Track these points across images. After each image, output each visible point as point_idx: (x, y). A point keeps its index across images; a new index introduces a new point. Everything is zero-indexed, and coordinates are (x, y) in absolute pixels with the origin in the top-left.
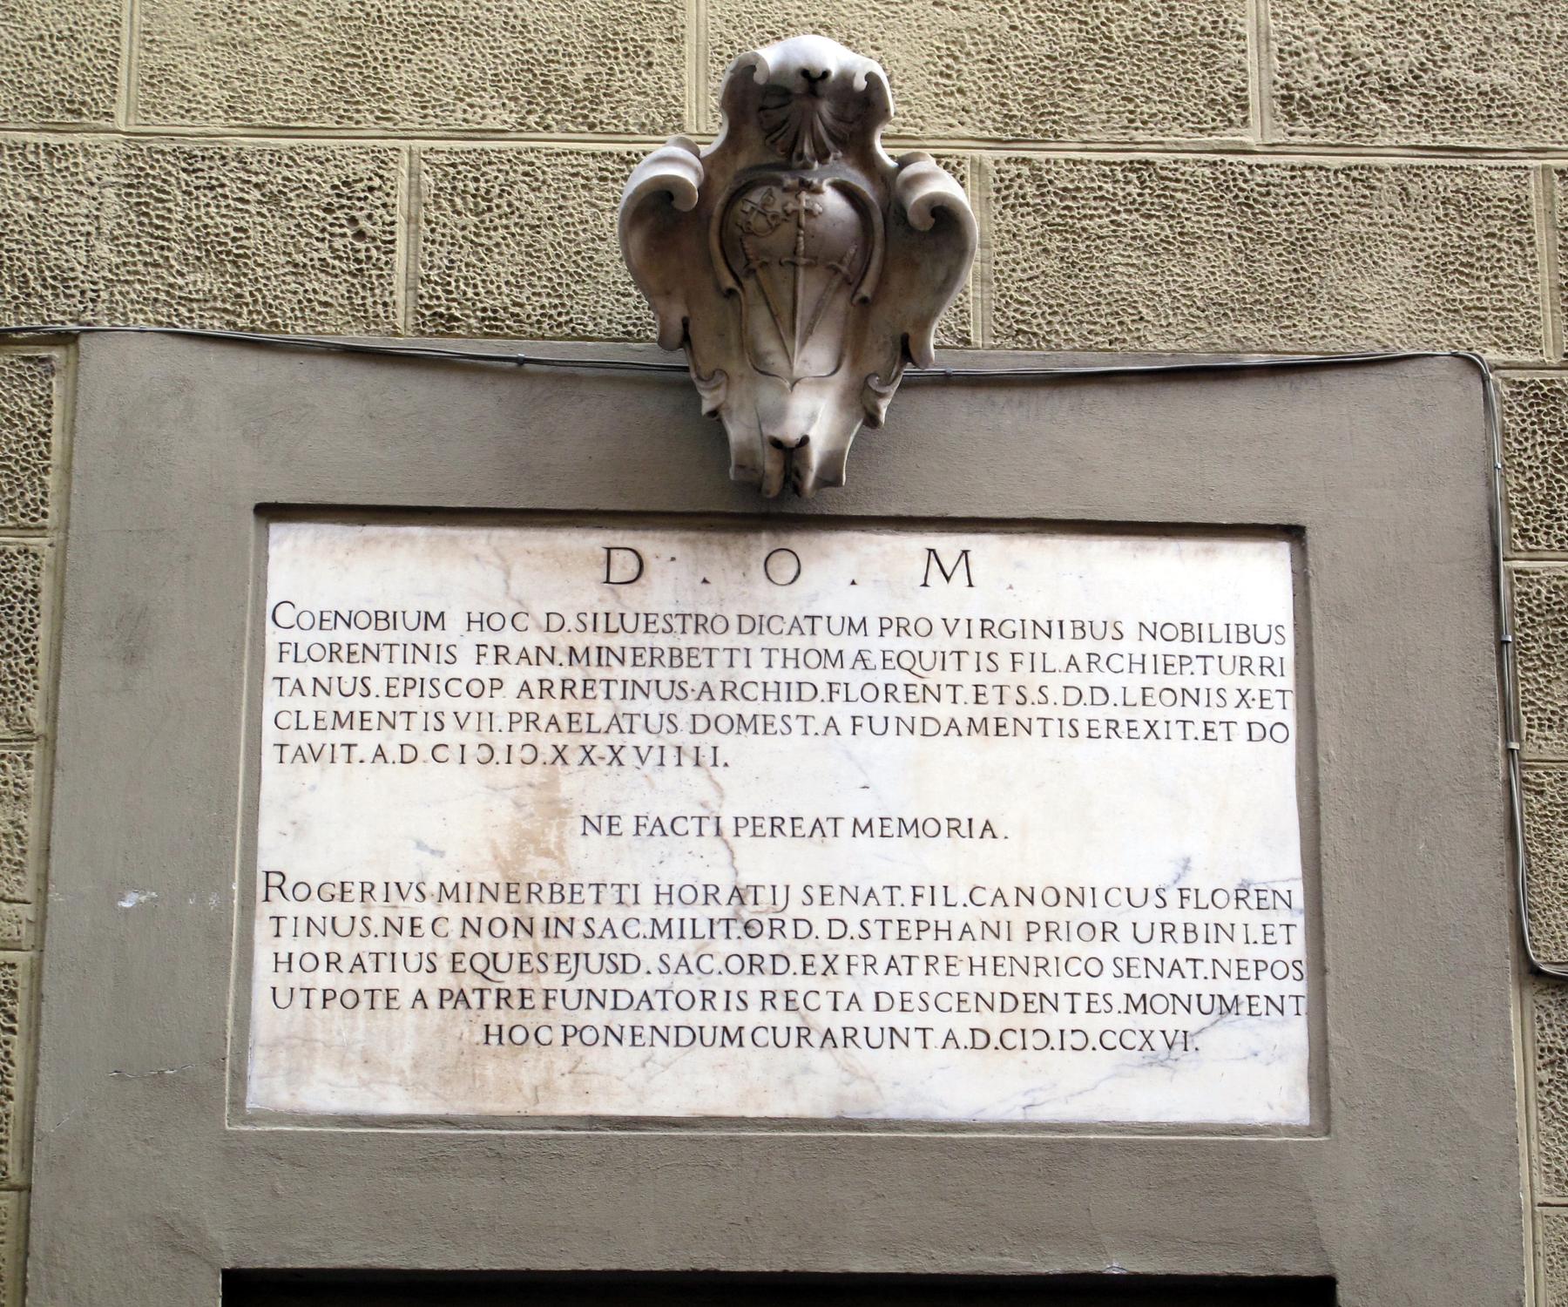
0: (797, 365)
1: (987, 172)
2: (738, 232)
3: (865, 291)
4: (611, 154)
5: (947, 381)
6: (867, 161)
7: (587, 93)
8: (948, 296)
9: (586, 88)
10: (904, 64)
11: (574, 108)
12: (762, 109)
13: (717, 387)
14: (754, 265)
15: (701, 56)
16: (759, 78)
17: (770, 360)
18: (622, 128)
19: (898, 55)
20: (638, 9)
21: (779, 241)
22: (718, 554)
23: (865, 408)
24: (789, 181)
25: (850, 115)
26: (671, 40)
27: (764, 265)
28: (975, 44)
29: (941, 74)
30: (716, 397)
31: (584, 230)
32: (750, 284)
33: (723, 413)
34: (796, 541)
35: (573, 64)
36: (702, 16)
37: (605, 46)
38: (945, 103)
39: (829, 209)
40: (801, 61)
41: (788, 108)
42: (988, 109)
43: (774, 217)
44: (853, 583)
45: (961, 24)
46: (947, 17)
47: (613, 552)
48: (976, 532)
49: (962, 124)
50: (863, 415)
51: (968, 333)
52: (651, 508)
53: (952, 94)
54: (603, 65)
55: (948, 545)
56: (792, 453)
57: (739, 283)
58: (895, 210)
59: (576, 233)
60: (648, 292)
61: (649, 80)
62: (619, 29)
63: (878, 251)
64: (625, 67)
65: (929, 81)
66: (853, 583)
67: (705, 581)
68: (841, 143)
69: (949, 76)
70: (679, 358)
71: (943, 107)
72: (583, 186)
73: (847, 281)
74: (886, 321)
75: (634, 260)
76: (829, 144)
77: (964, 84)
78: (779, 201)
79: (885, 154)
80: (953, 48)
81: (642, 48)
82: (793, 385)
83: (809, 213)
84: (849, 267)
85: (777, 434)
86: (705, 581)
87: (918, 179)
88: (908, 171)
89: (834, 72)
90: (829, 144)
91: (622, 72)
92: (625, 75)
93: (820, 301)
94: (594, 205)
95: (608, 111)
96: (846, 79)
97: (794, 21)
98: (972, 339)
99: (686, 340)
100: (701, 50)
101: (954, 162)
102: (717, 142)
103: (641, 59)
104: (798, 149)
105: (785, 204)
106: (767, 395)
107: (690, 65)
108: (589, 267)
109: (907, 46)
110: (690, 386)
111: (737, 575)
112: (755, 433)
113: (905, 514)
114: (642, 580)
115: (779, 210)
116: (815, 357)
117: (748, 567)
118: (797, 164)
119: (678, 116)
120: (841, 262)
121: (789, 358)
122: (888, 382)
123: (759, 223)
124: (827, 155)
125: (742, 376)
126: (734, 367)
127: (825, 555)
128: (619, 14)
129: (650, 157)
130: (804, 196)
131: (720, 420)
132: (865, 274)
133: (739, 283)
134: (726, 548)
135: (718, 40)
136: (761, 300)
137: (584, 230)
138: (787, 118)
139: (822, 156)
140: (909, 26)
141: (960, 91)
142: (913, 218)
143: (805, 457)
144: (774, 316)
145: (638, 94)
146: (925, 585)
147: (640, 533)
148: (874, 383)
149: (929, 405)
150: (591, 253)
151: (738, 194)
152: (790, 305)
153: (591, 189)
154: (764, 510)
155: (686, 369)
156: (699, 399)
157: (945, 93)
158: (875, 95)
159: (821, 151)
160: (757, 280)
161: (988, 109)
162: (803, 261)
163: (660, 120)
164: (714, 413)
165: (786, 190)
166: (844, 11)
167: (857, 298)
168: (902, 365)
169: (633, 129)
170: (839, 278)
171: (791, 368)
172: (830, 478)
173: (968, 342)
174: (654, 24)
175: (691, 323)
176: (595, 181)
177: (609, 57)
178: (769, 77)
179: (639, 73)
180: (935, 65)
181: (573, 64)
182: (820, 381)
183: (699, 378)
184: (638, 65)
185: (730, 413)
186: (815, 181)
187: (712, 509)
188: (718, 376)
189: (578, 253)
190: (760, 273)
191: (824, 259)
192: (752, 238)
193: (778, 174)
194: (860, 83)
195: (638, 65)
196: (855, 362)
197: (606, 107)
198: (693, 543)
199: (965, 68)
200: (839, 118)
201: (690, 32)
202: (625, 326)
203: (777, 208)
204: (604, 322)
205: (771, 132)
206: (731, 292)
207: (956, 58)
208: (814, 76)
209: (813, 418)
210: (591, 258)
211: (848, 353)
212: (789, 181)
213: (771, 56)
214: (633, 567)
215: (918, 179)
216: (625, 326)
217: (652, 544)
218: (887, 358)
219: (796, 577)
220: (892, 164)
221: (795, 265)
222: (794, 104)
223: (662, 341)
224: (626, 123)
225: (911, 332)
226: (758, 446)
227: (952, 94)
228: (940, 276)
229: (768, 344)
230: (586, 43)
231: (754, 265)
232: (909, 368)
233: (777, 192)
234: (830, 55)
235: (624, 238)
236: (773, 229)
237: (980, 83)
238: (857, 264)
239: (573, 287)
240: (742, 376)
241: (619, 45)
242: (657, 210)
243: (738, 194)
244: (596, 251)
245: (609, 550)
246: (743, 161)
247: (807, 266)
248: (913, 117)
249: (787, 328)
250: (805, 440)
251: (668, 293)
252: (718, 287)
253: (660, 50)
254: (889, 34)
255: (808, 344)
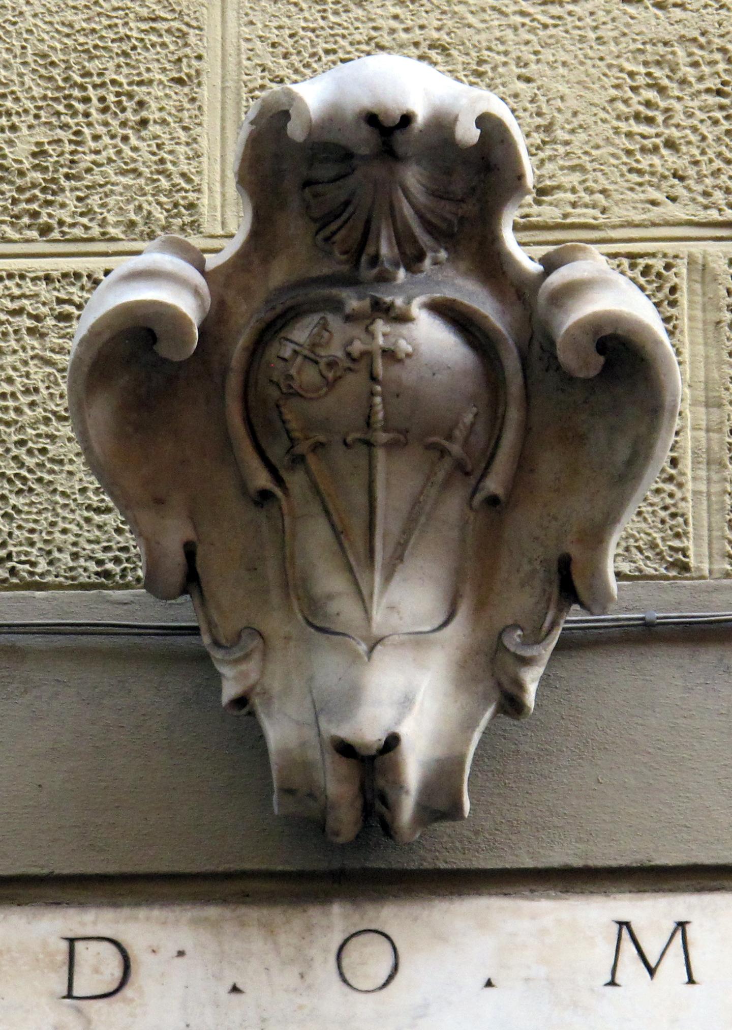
0: (378, 615)
1: (715, 279)
2: (274, 393)
3: (494, 484)
4: (78, 276)
5: (647, 634)
6: (491, 265)
7: (38, 176)
8: (634, 489)
9: (35, 167)
10: (573, 103)
11: (15, 201)
12: (308, 183)
13: (246, 657)
14: (302, 448)
15: (230, 105)
16: (296, 130)
17: (334, 607)
18: (96, 231)
19: (563, 89)
20: (122, 31)
21: (340, 404)
22: (258, 943)
23: (499, 684)
24: (354, 303)
25: (458, 187)
26: (180, 81)
27: (318, 446)
28: (695, 65)
29: (637, 117)
30: (244, 675)
31: (32, 405)
32: (296, 481)
33: (257, 701)
34: (393, 916)
35: (14, 128)
36: (232, 38)
37: (67, 96)
38: (644, 165)
39: (423, 348)
40: (364, 100)
41: (351, 182)
42: (716, 173)
43: (332, 364)
44: (489, 984)
45: (670, 32)
46: (648, 20)
47: (79, 946)
48: (700, 890)
49: (673, 199)
50: (496, 695)
51: (684, 551)
52: (142, 869)
53: (656, 149)
54: (65, 127)
55: (652, 913)
56: (373, 764)
57: (279, 480)
58: (537, 342)
59: (18, 410)
60: (125, 504)
61: (141, 149)
62: (93, 66)
63: (514, 415)
64: (100, 130)
65: (617, 131)
66: (489, 984)
67: (235, 989)
68: (444, 235)
69: (650, 121)
70: (183, 611)
71: (640, 172)
72: (31, 331)
73: (461, 469)
74: (532, 535)
75: (97, 448)
76: (424, 239)
77: (675, 133)
78: (340, 338)
79: (525, 257)
80: (657, 72)
81: (130, 96)
82: (371, 649)
83: (390, 355)
84: (466, 443)
85: (345, 732)
86: (235, 989)
87: (572, 290)
88: (557, 278)
89: (421, 114)
90: (424, 239)
91: (96, 138)
92: (101, 143)
93: (416, 504)
94: (48, 362)
95: (72, 203)
96: (442, 125)
97: (386, 40)
98: (692, 562)
99: (192, 581)
100: (230, 95)
101: (658, 264)
102: (231, 248)
103: (129, 114)
104: (370, 250)
105: (351, 342)
106: (328, 667)
107: (211, 120)
108: (41, 465)
109: (578, 74)
110: (203, 658)
111: (290, 977)
112: (310, 734)
113: (577, 862)
114: (128, 992)
115: (340, 354)
116: (410, 599)
117: (309, 962)
118: (368, 273)
119: (191, 206)
120: (450, 437)
121: (364, 601)
122: (536, 637)
123: (310, 375)
124: (421, 257)
125: (287, 638)
126: (275, 624)
127: (441, 938)
128: (91, 41)
129: (111, 276)
130: (381, 326)
131: (252, 714)
132: (493, 456)
133: (279, 480)
134: (269, 930)
135: (258, 78)
136: (316, 509)
137: (32, 405)
138: (353, 197)
139: (412, 259)
140: (582, 39)
141: (670, 144)
142: (566, 357)
143: (394, 771)
144: (338, 533)
145: (124, 173)
146: (612, 983)
147: (126, 912)
148: (513, 640)
149: (617, 678)
150: (43, 443)
151: (272, 329)
152: (364, 512)
153: (43, 336)
154: (336, 865)
155: (195, 631)
156: (217, 678)
157: (643, 150)
158: (498, 153)
159: (410, 250)
160: (308, 472)
161: (716, 173)
162: (382, 437)
163: (160, 215)
164: (241, 702)
165: (349, 318)
166: (471, 19)
167: (479, 497)
168: (562, 609)
169: (113, 231)
170: (447, 464)
171: (368, 617)
172: (441, 803)
173: (685, 568)
174: (151, 55)
175: (200, 551)
176: (50, 322)
177: (75, 114)
178: (312, 129)
179: (125, 139)
180: (626, 102)
181: (14, 128)
182: (418, 641)
183: (216, 643)
184: (124, 124)
185: (268, 700)
186: (399, 302)
187: (248, 866)
188: (250, 639)
189: (21, 443)
190: (311, 460)
191: (419, 432)
192: (294, 402)
193: (335, 291)
194: (468, 133)
195: (124, 124)
196: (481, 606)
197: (69, 198)
198: (215, 926)
199: (678, 106)
200: (438, 194)
201: (211, 68)
202: (100, 562)
203: (336, 351)
204: (66, 557)
205: (324, 221)
206: (265, 496)
207: (662, 90)
208: (389, 123)
209: (406, 702)
210: (43, 451)
211: (467, 589)
212: (354, 303)
213: (314, 94)
214: (113, 969)
215: (572, 290)
216: (100, 562)
217: (147, 930)
218: (535, 590)
219: (391, 978)
220: (534, 268)
221: (369, 444)
222: (358, 174)
223: (151, 583)
224: (103, 223)
225: (574, 551)
226: (314, 754)
227: (656, 149)
228: (623, 452)
229: (330, 582)
230: (37, 92)
231: (302, 448)
232: (575, 615)
233: (335, 322)
234: (415, 87)
235: (78, 412)
236: (331, 385)
237: (704, 129)
238: (480, 439)
239: (13, 500)
240: (287, 638)
241: (91, 92)
242: (133, 363)
243: (272, 329)
244: (52, 438)
245: (72, 941)
246: (279, 273)
247: (391, 446)
248: (589, 191)
249: (359, 551)
250: (392, 742)
251: (159, 501)
252: (243, 486)
253: (160, 98)
254: (547, 55)
255: (397, 578)
